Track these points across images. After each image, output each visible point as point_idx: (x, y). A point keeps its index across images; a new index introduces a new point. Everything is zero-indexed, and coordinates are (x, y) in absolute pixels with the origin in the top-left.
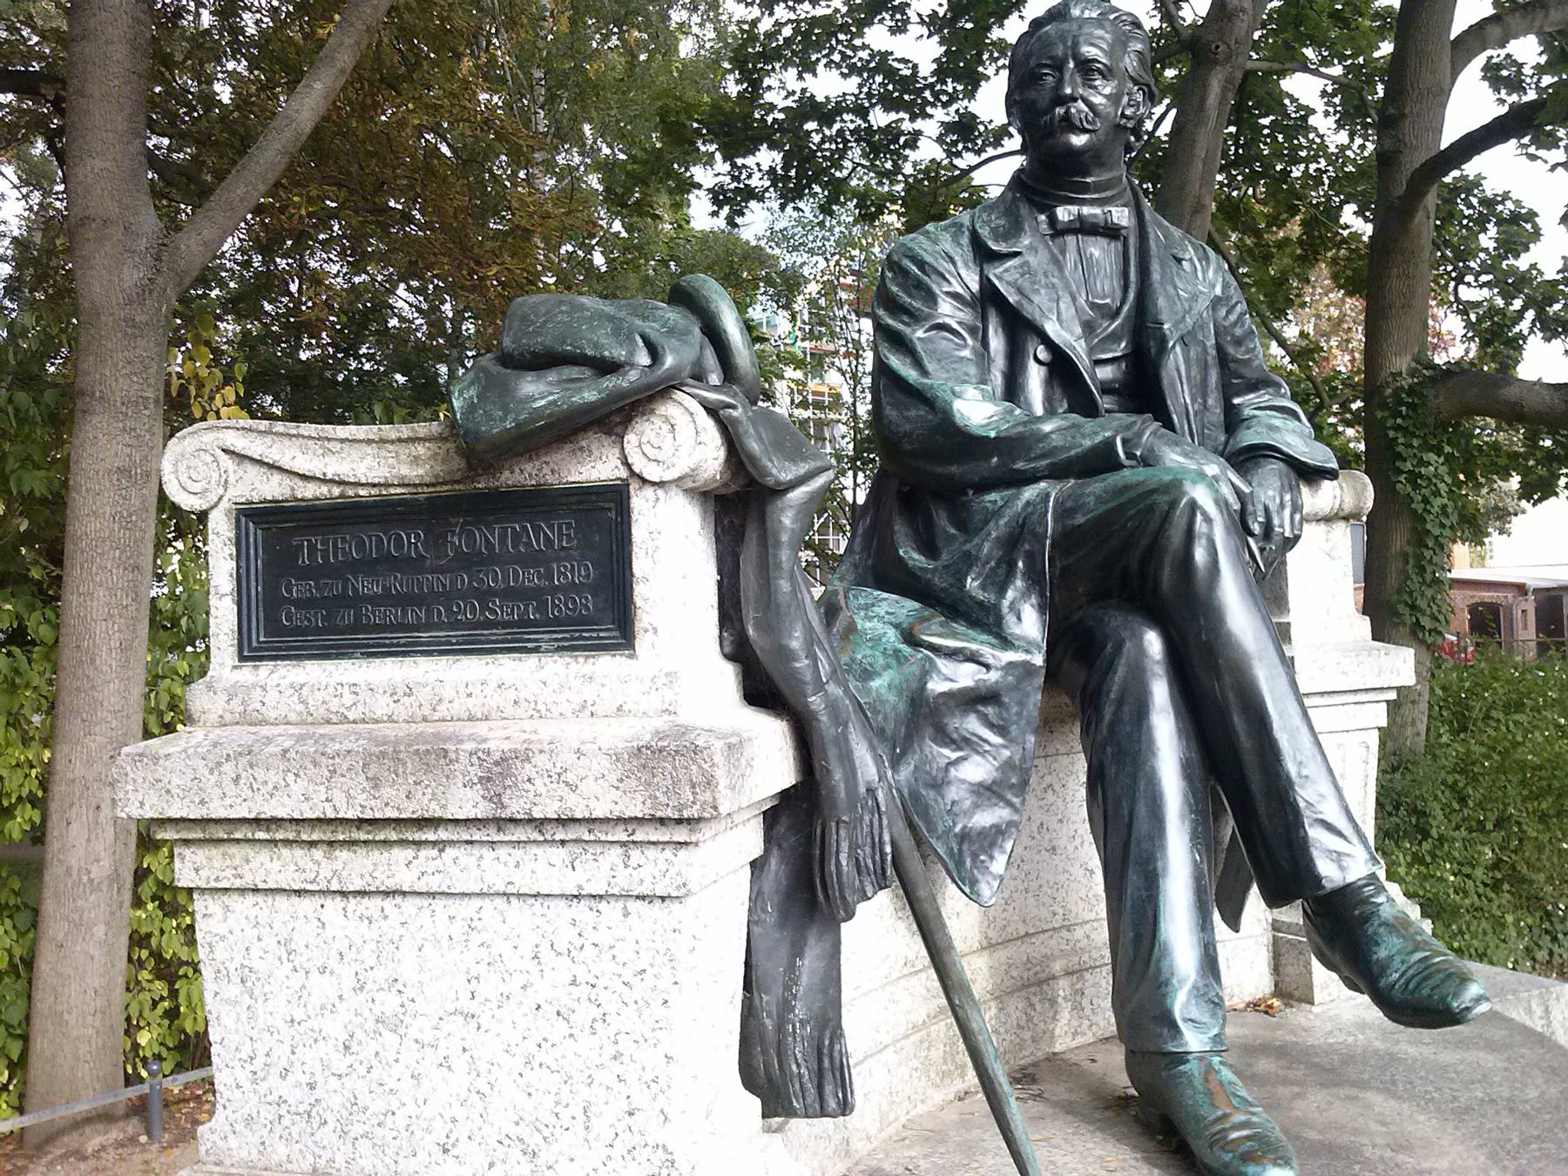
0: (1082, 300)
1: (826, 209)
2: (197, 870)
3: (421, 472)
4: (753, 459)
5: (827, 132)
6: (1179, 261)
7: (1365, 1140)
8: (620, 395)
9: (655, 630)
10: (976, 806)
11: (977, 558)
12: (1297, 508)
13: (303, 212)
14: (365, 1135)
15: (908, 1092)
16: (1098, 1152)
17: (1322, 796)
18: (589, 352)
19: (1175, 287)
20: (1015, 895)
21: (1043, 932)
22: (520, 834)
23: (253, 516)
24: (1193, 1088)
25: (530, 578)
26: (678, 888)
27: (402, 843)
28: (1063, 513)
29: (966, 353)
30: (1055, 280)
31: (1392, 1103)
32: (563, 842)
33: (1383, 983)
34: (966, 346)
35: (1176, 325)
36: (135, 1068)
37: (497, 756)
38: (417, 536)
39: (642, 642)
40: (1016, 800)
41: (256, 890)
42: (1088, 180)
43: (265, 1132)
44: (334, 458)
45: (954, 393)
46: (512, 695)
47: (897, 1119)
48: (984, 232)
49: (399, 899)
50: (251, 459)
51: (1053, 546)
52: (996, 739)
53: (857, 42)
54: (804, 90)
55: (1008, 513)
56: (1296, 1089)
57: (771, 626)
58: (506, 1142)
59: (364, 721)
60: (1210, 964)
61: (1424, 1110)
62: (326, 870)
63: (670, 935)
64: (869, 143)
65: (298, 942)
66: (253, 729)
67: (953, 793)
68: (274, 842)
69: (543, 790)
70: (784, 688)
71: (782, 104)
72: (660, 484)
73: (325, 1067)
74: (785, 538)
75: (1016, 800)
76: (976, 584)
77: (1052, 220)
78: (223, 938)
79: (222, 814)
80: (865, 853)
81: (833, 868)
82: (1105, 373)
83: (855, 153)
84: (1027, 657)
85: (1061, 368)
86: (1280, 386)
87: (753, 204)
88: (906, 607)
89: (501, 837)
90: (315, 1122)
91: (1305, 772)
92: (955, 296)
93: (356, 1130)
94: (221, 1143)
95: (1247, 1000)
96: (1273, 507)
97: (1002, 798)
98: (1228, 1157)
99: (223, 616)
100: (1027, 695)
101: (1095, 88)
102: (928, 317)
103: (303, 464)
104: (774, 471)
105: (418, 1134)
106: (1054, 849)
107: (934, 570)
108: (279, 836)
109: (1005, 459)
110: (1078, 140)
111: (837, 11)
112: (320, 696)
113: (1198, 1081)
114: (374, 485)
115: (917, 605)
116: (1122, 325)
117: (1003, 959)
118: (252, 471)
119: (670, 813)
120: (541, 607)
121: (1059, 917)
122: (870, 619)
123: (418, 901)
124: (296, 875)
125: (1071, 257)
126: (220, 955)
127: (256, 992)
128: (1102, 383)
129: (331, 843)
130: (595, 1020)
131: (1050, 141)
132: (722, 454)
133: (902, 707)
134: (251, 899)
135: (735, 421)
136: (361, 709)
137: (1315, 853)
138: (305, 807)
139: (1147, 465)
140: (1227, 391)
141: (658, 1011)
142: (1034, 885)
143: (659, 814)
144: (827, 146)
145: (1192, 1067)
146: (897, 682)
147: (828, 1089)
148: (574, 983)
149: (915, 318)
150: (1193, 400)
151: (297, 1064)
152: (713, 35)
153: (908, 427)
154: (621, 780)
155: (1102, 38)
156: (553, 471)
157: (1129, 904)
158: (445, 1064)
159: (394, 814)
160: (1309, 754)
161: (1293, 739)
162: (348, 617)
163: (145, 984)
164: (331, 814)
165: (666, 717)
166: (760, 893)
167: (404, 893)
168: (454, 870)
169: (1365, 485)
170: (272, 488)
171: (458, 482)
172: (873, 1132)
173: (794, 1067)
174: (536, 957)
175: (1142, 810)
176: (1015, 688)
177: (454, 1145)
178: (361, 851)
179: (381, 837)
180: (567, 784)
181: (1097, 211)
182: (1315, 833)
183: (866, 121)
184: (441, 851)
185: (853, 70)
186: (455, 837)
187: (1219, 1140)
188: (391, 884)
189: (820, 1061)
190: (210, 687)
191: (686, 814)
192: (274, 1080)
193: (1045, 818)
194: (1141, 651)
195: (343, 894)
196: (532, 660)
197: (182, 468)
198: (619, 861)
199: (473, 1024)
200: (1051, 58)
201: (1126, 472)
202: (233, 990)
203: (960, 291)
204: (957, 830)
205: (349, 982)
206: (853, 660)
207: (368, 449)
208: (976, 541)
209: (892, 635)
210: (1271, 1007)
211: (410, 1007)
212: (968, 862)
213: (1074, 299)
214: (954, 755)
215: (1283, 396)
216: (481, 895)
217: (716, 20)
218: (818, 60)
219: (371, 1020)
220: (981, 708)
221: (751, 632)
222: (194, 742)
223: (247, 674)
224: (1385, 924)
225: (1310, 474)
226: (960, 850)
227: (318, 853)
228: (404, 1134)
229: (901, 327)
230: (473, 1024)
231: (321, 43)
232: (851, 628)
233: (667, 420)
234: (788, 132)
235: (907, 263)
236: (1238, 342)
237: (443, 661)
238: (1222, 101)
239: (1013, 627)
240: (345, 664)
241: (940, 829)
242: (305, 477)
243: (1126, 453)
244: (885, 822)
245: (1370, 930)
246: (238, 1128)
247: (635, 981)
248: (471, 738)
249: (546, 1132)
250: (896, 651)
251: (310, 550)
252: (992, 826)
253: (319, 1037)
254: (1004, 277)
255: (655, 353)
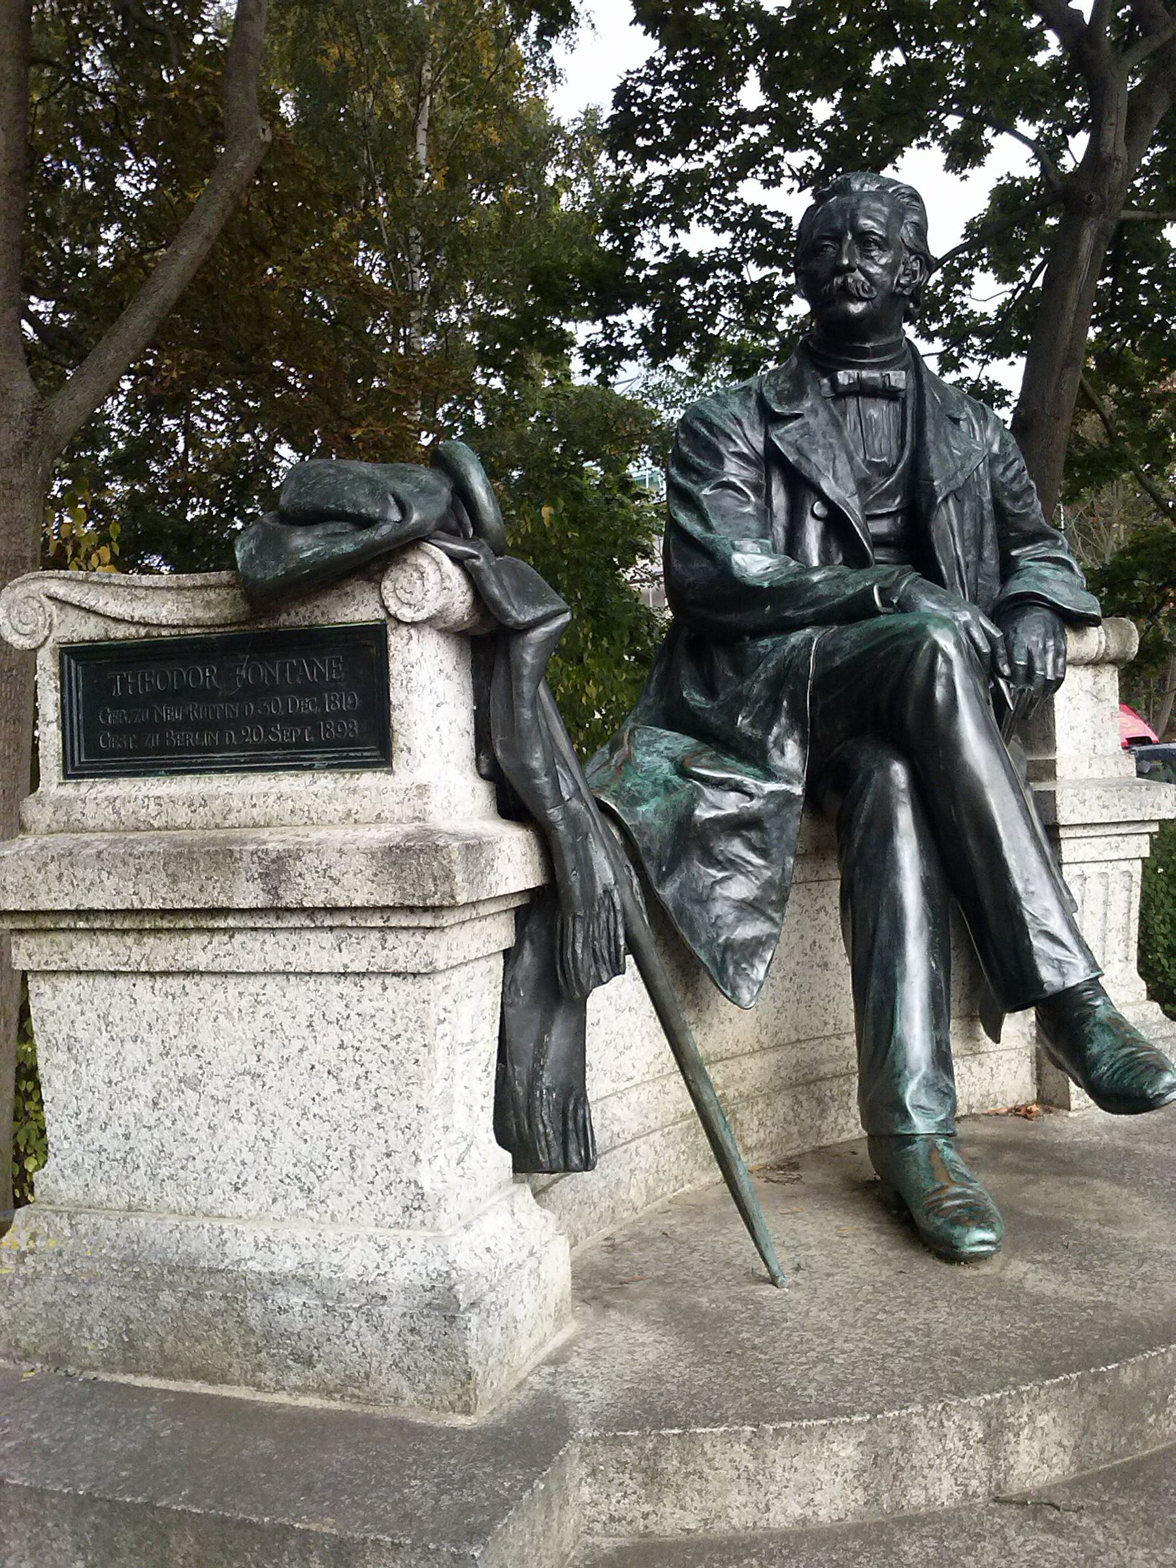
0: (859, 459)
1: (698, 366)
2: (30, 956)
3: (212, 614)
4: (495, 603)
5: (700, 288)
6: (956, 421)
7: (1079, 1217)
8: (372, 546)
9: (409, 750)
10: (739, 920)
11: (748, 698)
12: (1059, 653)
13: (175, 375)
14: (171, 1177)
15: (675, 1172)
16: (837, 1222)
17: (1047, 910)
18: (349, 510)
19: (949, 446)
20: (787, 1005)
21: (814, 1039)
22: (295, 921)
23: (75, 655)
24: (918, 1166)
25: (306, 706)
26: (426, 966)
27: (198, 930)
28: (824, 655)
29: (748, 509)
30: (833, 441)
31: (1116, 1189)
32: (331, 928)
33: (1094, 1074)
34: (749, 502)
35: (947, 481)
36: (22, 1192)
37: (274, 855)
38: (211, 671)
39: (398, 761)
40: (776, 916)
41: (79, 972)
42: (867, 345)
43: (88, 1176)
44: (140, 604)
45: (734, 547)
46: (289, 805)
47: (664, 1194)
48: (770, 395)
49: (197, 978)
50: (71, 605)
51: (814, 687)
52: (760, 862)
53: (730, 196)
54: (676, 246)
55: (776, 657)
56: (1031, 1177)
57: (517, 749)
58: (287, 1181)
59: (167, 828)
60: (942, 1060)
61: (1140, 1194)
62: (136, 955)
63: (421, 1006)
64: (743, 299)
65: (115, 1016)
66: (75, 836)
67: (718, 908)
68: (93, 931)
69: (311, 884)
70: (528, 803)
71: (654, 261)
72: (413, 624)
73: (138, 1118)
74: (526, 672)
75: (776, 916)
76: (746, 722)
77: (834, 382)
78: (52, 1013)
79: (49, 906)
80: (602, 945)
81: (569, 956)
82: (880, 527)
83: (727, 311)
84: (788, 787)
85: (836, 524)
86: (1057, 538)
87: (625, 363)
88: (679, 743)
89: (279, 924)
90: (129, 1167)
91: (1031, 888)
92: (740, 455)
93: (164, 1172)
94: (53, 1186)
95: (1011, 1106)
96: (1036, 652)
97: (762, 913)
98: (939, 1222)
99: (50, 737)
100: (788, 821)
101: (872, 258)
102: (715, 475)
103: (115, 608)
104: (514, 613)
105: (214, 1176)
106: (826, 965)
107: (712, 709)
108: (97, 925)
109: (777, 605)
110: (856, 308)
111: (709, 165)
112: (130, 807)
113: (922, 1159)
114: (174, 627)
115: (693, 741)
116: (896, 482)
117: (773, 1062)
118: (73, 615)
119: (415, 902)
120: (315, 732)
121: (830, 1027)
122: (650, 754)
123: (213, 979)
124: (111, 959)
125: (852, 417)
126: (49, 1028)
127: (80, 1059)
128: (874, 536)
129: (140, 931)
130: (358, 1077)
131: (830, 309)
132: (468, 598)
133: (667, 830)
134: (75, 980)
135: (478, 570)
136: (164, 819)
137: (1038, 961)
138: (117, 899)
139: (904, 611)
140: (1004, 545)
141: (411, 1067)
142: (807, 996)
143: (407, 903)
144: (700, 302)
145: (919, 1147)
146: (663, 808)
147: (572, 1147)
148: (342, 1046)
149: (703, 476)
150: (965, 554)
151: (115, 1118)
152: (588, 190)
153: (692, 579)
154: (375, 875)
155: (880, 211)
156: (323, 614)
157: (871, 1006)
158: (237, 1117)
159: (190, 905)
160: (1035, 872)
161: (1021, 859)
162: (155, 741)
163: (32, 1115)
164: (137, 905)
165: (417, 823)
166: (513, 980)
167: (201, 973)
168: (242, 954)
169: (1131, 632)
170: (89, 630)
171: (243, 623)
172: (639, 1204)
173: (541, 1127)
174: (310, 1025)
175: (884, 923)
176: (776, 814)
177: (244, 1184)
178: (165, 937)
179: (180, 925)
180: (331, 878)
181: (876, 374)
182: (1039, 944)
183: (739, 276)
184: (231, 937)
185: (726, 225)
186: (241, 925)
187: (935, 1208)
188: (189, 965)
189: (565, 1124)
190: (39, 801)
191: (429, 902)
192: (95, 1132)
193: (818, 937)
194: (888, 780)
195: (152, 974)
196: (307, 777)
197: (14, 613)
198: (377, 944)
199: (259, 1083)
200: (831, 230)
201: (882, 618)
202: (61, 1057)
203: (746, 450)
204: (721, 940)
205: (156, 1049)
206: (622, 788)
207: (169, 596)
208: (748, 682)
209: (666, 766)
210: (1030, 1112)
211: (207, 1068)
212: (731, 970)
213: (851, 459)
214: (720, 875)
215: (1060, 548)
216: (265, 973)
217: (591, 176)
218: (691, 215)
219: (175, 1079)
220: (745, 833)
221: (499, 753)
222: (26, 846)
223: (69, 790)
224: (1100, 1024)
225: (1078, 622)
226: (723, 961)
227: (129, 940)
228: (204, 1175)
229: (690, 485)
230: (259, 1083)
231: (190, 207)
232: (628, 760)
233: (417, 568)
234: (660, 289)
235: (697, 425)
236: (1015, 497)
237: (233, 777)
238: (1096, 249)
239: (776, 760)
240: (152, 780)
241: (703, 938)
242: (116, 620)
243: (881, 600)
244: (620, 919)
245: (1087, 1029)
246: (68, 1172)
247: (392, 1045)
248: (253, 841)
249: (319, 1172)
250: (667, 782)
251: (121, 683)
252: (754, 938)
253: (133, 1095)
254: (785, 438)
255: (404, 510)
